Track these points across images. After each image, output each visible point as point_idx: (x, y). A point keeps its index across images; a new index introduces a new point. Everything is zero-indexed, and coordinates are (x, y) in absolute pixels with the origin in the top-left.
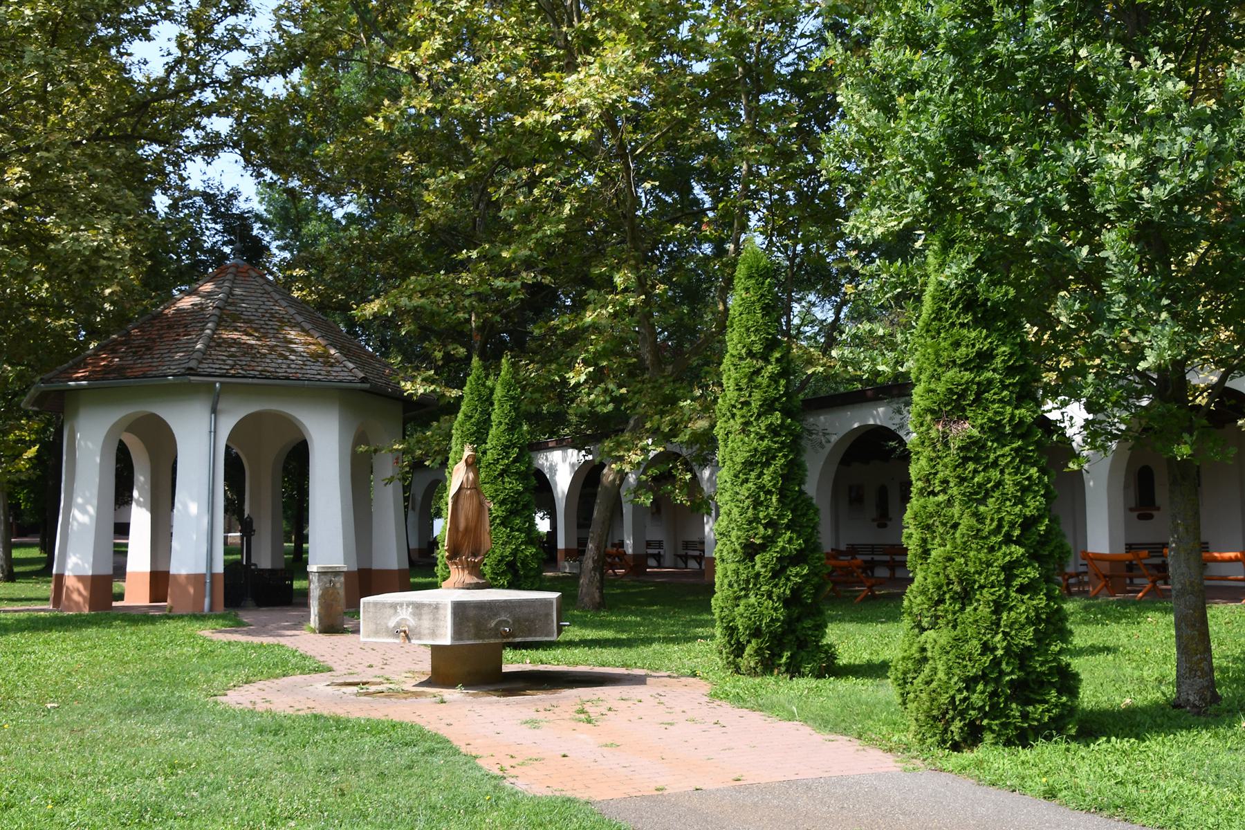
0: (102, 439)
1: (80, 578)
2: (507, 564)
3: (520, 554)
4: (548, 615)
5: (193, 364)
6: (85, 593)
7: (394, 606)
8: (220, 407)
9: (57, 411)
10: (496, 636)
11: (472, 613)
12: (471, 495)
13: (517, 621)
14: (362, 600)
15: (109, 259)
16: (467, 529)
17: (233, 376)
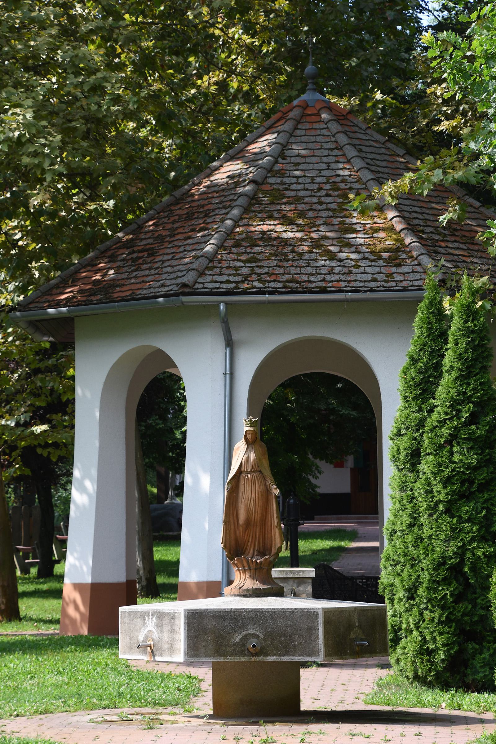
0: (101, 386)
1: (78, 587)
2: (452, 568)
3: (469, 555)
4: (312, 630)
5: (188, 279)
6: (82, 608)
7: (143, 615)
8: (236, 336)
9: (57, 344)
10: (242, 654)
11: (210, 624)
12: (253, 480)
13: (269, 635)
14: (121, 609)
15: (36, 154)
16: (248, 523)
17: (245, 292)
